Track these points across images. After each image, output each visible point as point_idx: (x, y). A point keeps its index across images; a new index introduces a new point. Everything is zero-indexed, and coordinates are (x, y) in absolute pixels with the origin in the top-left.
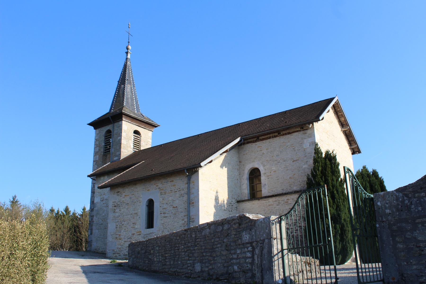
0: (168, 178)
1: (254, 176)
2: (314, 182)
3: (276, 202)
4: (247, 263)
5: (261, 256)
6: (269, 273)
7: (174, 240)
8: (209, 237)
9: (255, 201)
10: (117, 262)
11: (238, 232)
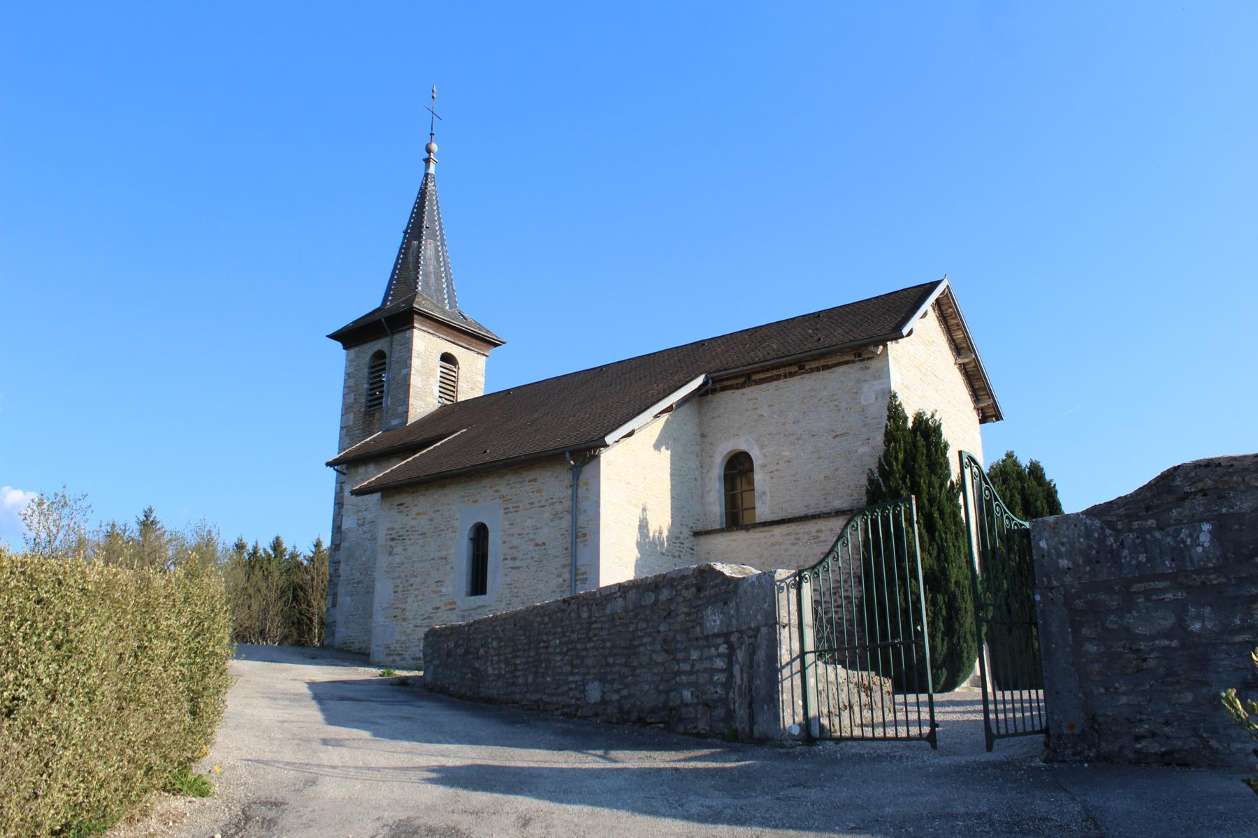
0: (525, 473)
4: (715, 684)
5: (751, 666)
7: (536, 624)
9: (738, 533)
10: (396, 675)
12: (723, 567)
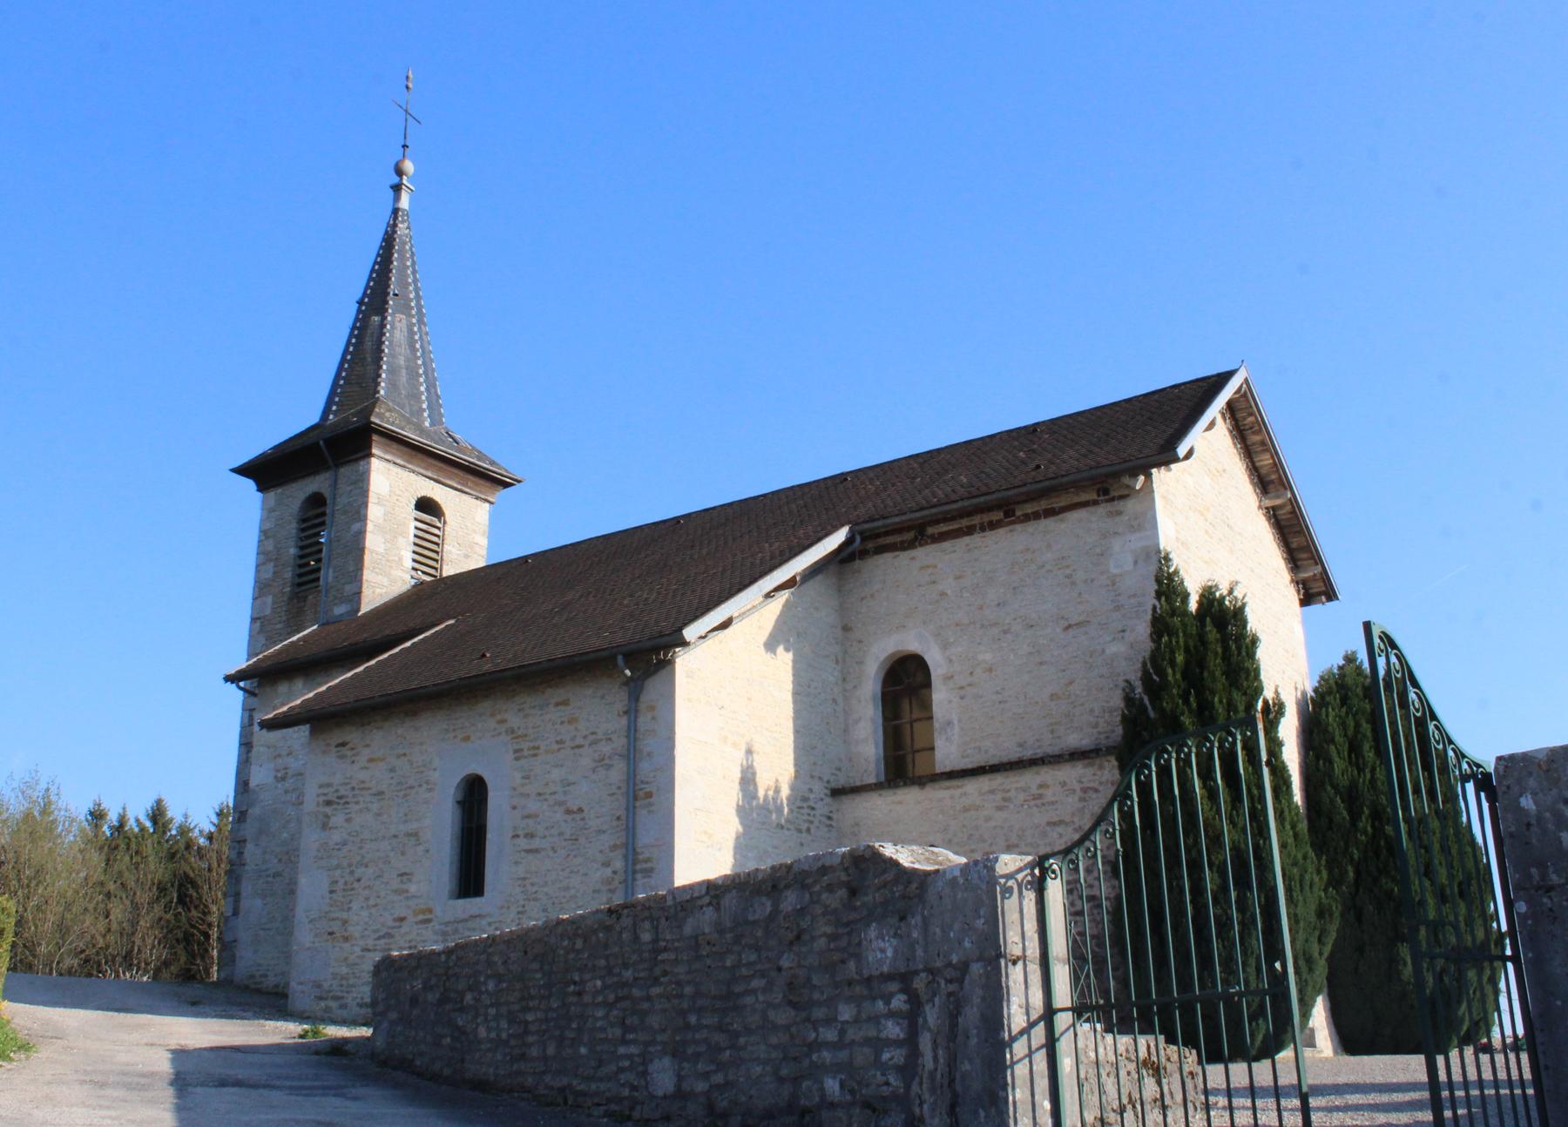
1: (902, 687)
2: (1152, 714)
3: (992, 797)
4: (884, 1068)
6: (986, 1117)
7: (562, 952)
8: (714, 945)
10: (326, 1035)
11: (847, 924)
12: (897, 851)
